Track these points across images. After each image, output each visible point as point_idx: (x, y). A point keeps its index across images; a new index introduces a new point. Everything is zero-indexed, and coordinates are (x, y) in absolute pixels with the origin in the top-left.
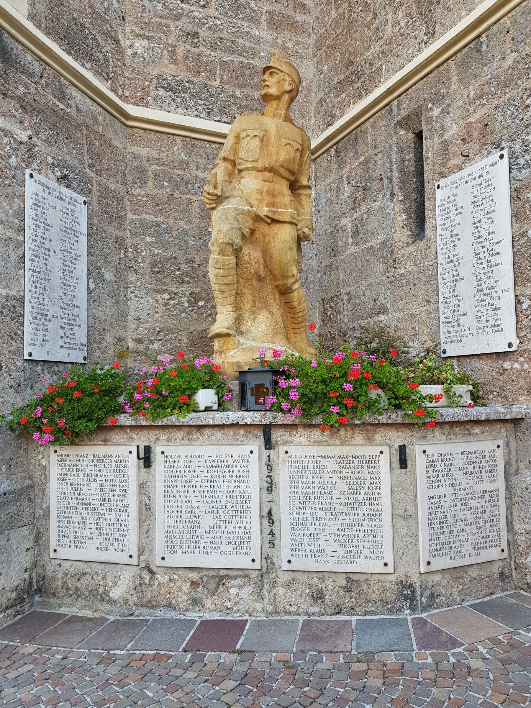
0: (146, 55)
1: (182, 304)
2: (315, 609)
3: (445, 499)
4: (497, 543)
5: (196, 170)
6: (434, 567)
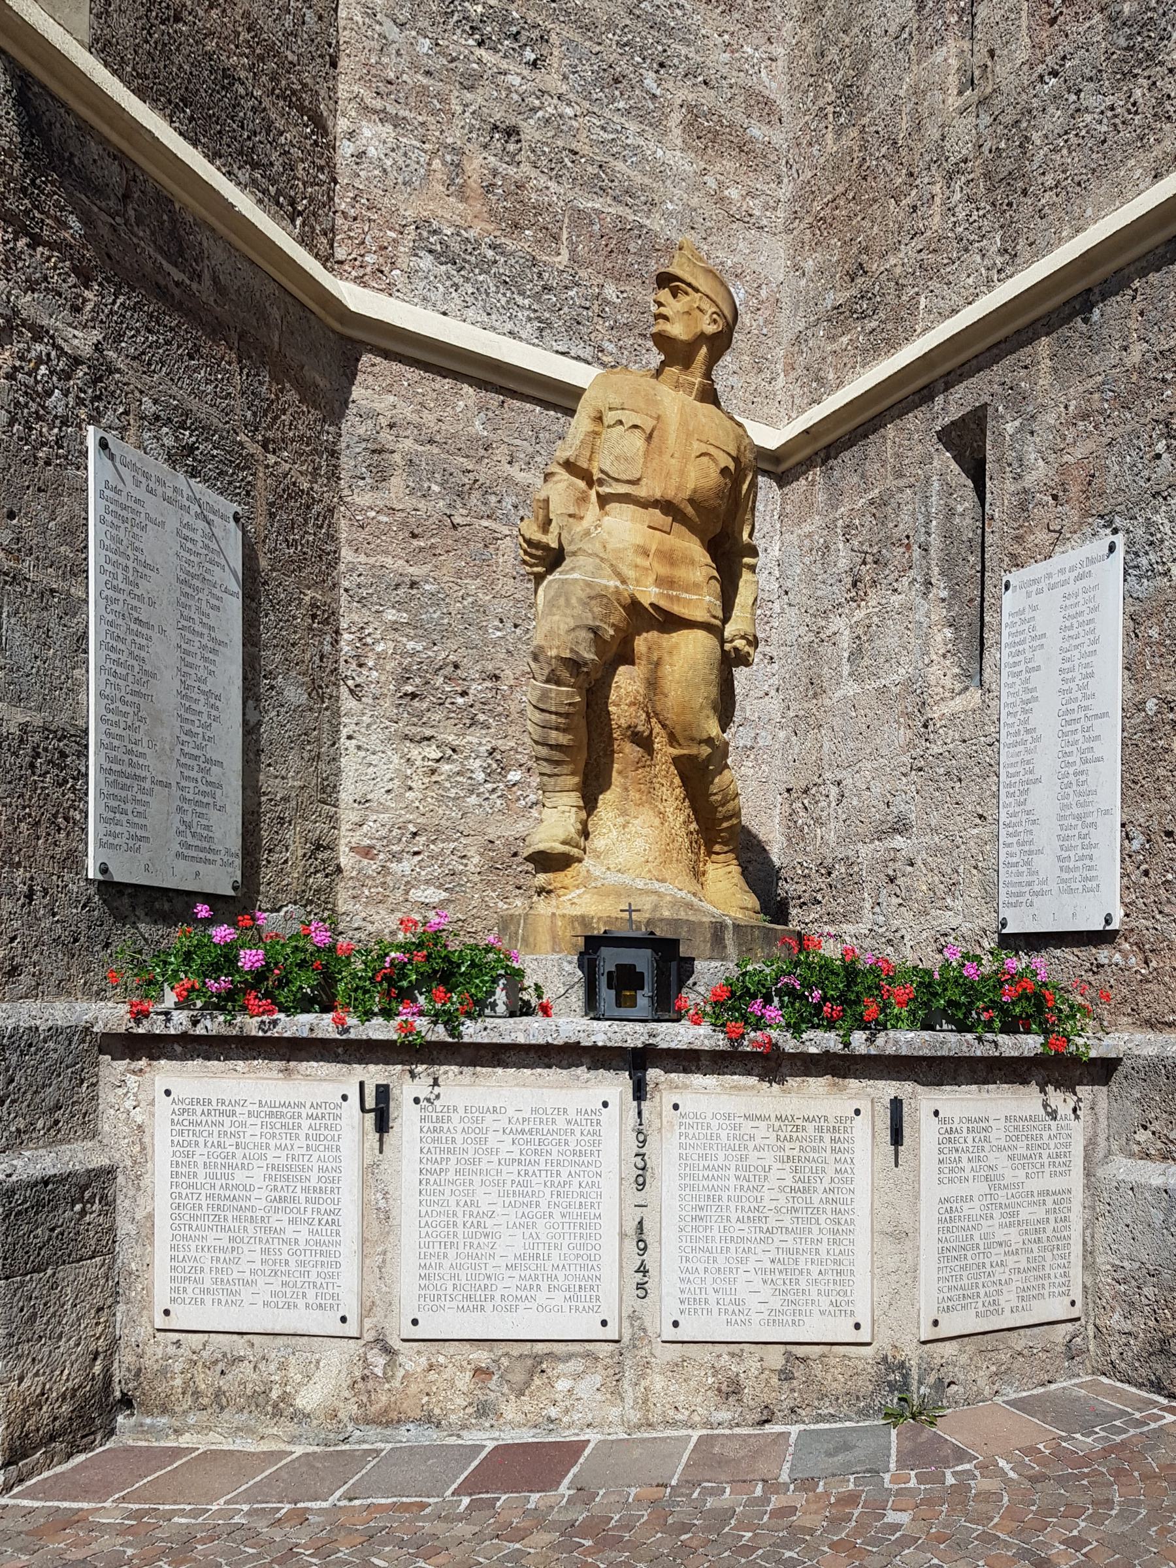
0: (389, 162)
1: (469, 775)
2: (724, 1415)
3: (971, 1204)
4: (1064, 1289)
5: (509, 463)
6: (943, 1331)
